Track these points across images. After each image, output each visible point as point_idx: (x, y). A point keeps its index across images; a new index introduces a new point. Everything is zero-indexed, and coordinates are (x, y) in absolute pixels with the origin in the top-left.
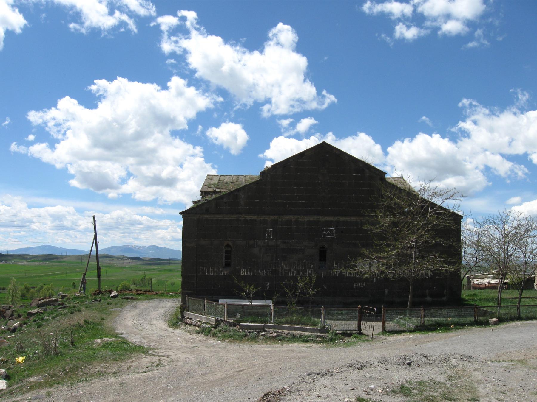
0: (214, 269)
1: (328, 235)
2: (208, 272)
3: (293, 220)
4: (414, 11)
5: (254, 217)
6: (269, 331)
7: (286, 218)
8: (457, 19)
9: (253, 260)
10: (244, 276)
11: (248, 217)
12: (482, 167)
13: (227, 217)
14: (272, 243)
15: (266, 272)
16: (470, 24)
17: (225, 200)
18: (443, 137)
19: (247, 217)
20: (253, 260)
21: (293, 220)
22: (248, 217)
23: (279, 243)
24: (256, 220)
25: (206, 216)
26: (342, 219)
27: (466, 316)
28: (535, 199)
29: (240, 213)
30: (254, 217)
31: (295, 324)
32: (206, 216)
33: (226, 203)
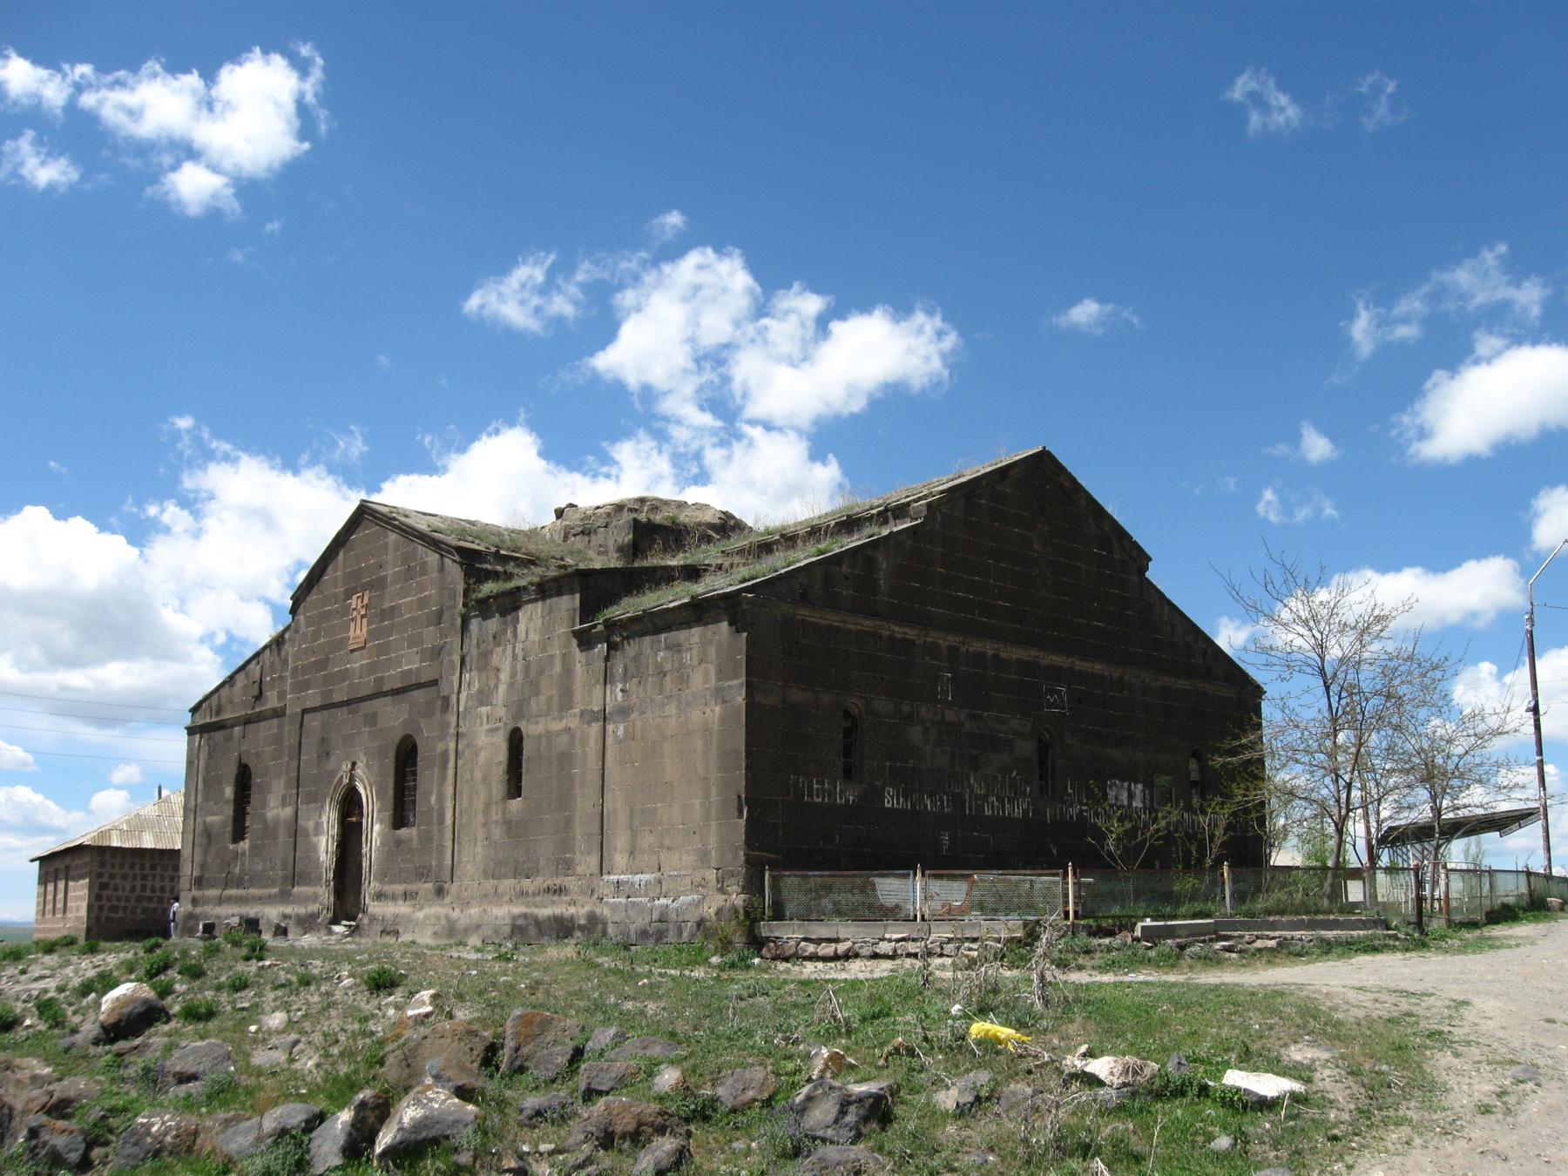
0: (822, 783)
1: (1055, 705)
2: (810, 795)
3: (990, 653)
4: (71, 107)
5: (911, 633)
6: (1242, 937)
7: (977, 646)
8: (214, 169)
9: (911, 763)
10: (892, 810)
11: (899, 631)
12: (221, 638)
13: (854, 624)
14: (950, 716)
15: (941, 800)
16: (247, 188)
17: (845, 569)
18: (104, 527)
19: (897, 629)
20: (911, 763)
21: (990, 653)
22: (899, 631)
23: (962, 717)
24: (913, 642)
25: (803, 613)
26: (1080, 665)
27: (1115, 985)
28: (1561, 647)
29: (877, 615)
30: (911, 633)
31: (1298, 914)
32: (803, 613)
33: (847, 578)
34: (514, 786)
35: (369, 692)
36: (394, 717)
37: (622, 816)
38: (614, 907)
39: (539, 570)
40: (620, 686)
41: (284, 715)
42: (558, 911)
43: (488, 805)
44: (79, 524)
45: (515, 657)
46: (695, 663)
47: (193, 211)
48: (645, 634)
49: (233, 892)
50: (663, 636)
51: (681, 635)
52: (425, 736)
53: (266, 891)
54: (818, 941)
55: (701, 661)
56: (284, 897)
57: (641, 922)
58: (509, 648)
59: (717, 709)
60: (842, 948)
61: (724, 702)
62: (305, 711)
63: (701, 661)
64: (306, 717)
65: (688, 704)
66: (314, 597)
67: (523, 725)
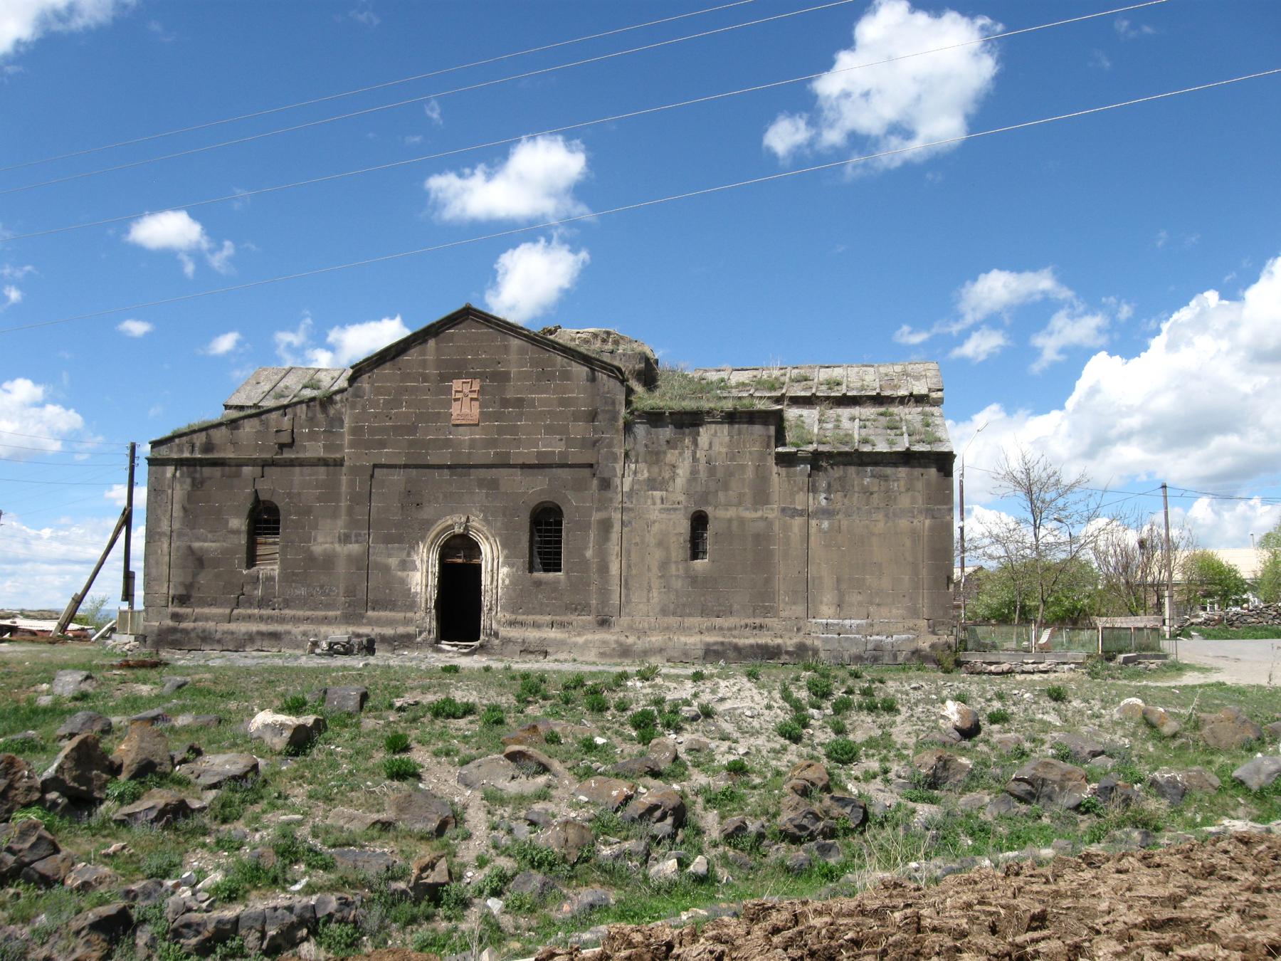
34: (696, 548)
35: (489, 462)
36: (534, 489)
37: (829, 581)
38: (826, 641)
39: (1233, 440)
40: (823, 495)
41: (342, 465)
42: (761, 641)
43: (664, 565)
44: (1143, 354)
45: (695, 459)
46: (903, 489)
47: (781, 117)
48: (850, 464)
49: (383, 614)
50: (869, 469)
51: (889, 471)
52: (572, 504)
53: (331, 613)
54: (991, 664)
55: (908, 490)
56: (348, 619)
57: (854, 650)
58: (688, 453)
59: (927, 522)
60: (1005, 667)
61: (933, 517)
62: (375, 466)
63: (908, 490)
64: (377, 470)
65: (894, 514)
66: (387, 370)
67: (709, 510)
